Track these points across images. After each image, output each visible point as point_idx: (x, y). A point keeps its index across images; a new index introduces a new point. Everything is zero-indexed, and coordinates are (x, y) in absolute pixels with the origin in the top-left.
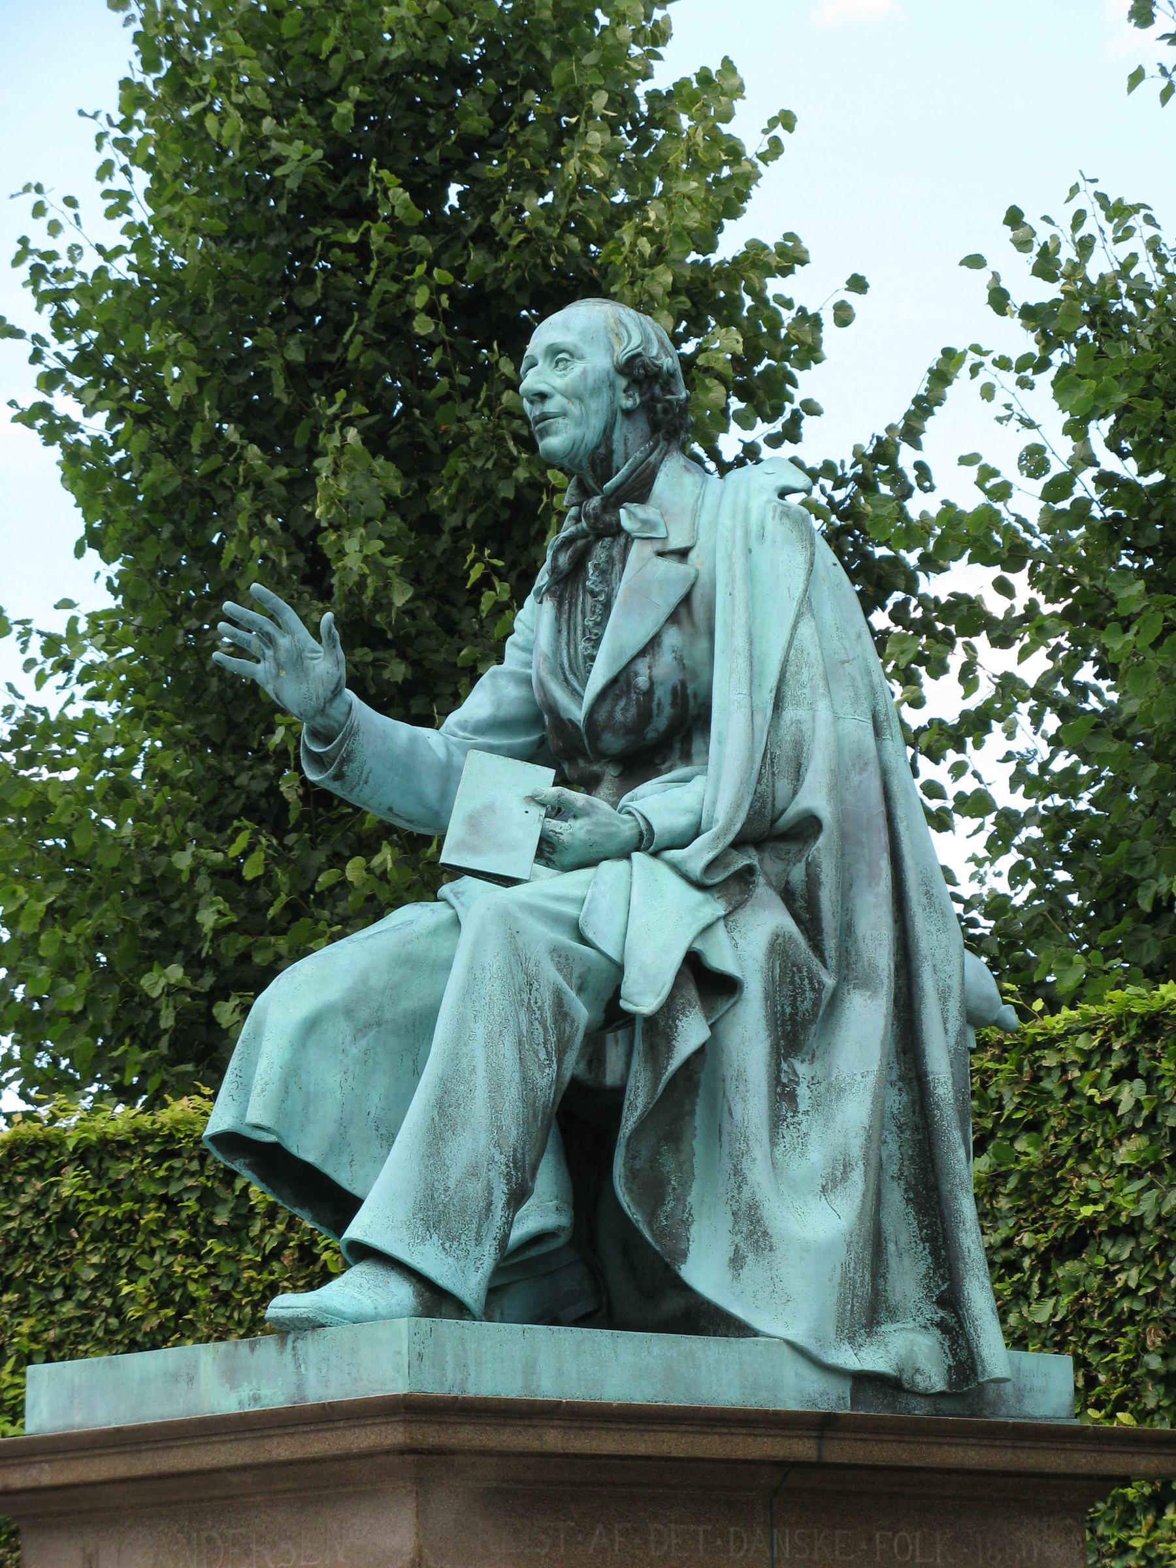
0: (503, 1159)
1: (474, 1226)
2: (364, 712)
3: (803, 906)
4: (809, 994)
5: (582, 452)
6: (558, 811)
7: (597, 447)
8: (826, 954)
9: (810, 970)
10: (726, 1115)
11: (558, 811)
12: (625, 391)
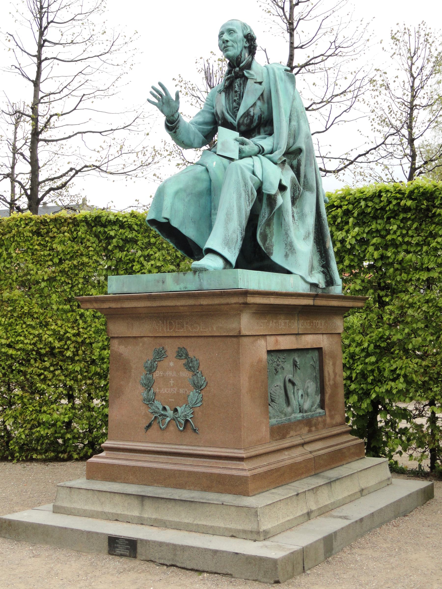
3: (297, 170)
4: (298, 192)
6: (243, 143)
11: (243, 143)
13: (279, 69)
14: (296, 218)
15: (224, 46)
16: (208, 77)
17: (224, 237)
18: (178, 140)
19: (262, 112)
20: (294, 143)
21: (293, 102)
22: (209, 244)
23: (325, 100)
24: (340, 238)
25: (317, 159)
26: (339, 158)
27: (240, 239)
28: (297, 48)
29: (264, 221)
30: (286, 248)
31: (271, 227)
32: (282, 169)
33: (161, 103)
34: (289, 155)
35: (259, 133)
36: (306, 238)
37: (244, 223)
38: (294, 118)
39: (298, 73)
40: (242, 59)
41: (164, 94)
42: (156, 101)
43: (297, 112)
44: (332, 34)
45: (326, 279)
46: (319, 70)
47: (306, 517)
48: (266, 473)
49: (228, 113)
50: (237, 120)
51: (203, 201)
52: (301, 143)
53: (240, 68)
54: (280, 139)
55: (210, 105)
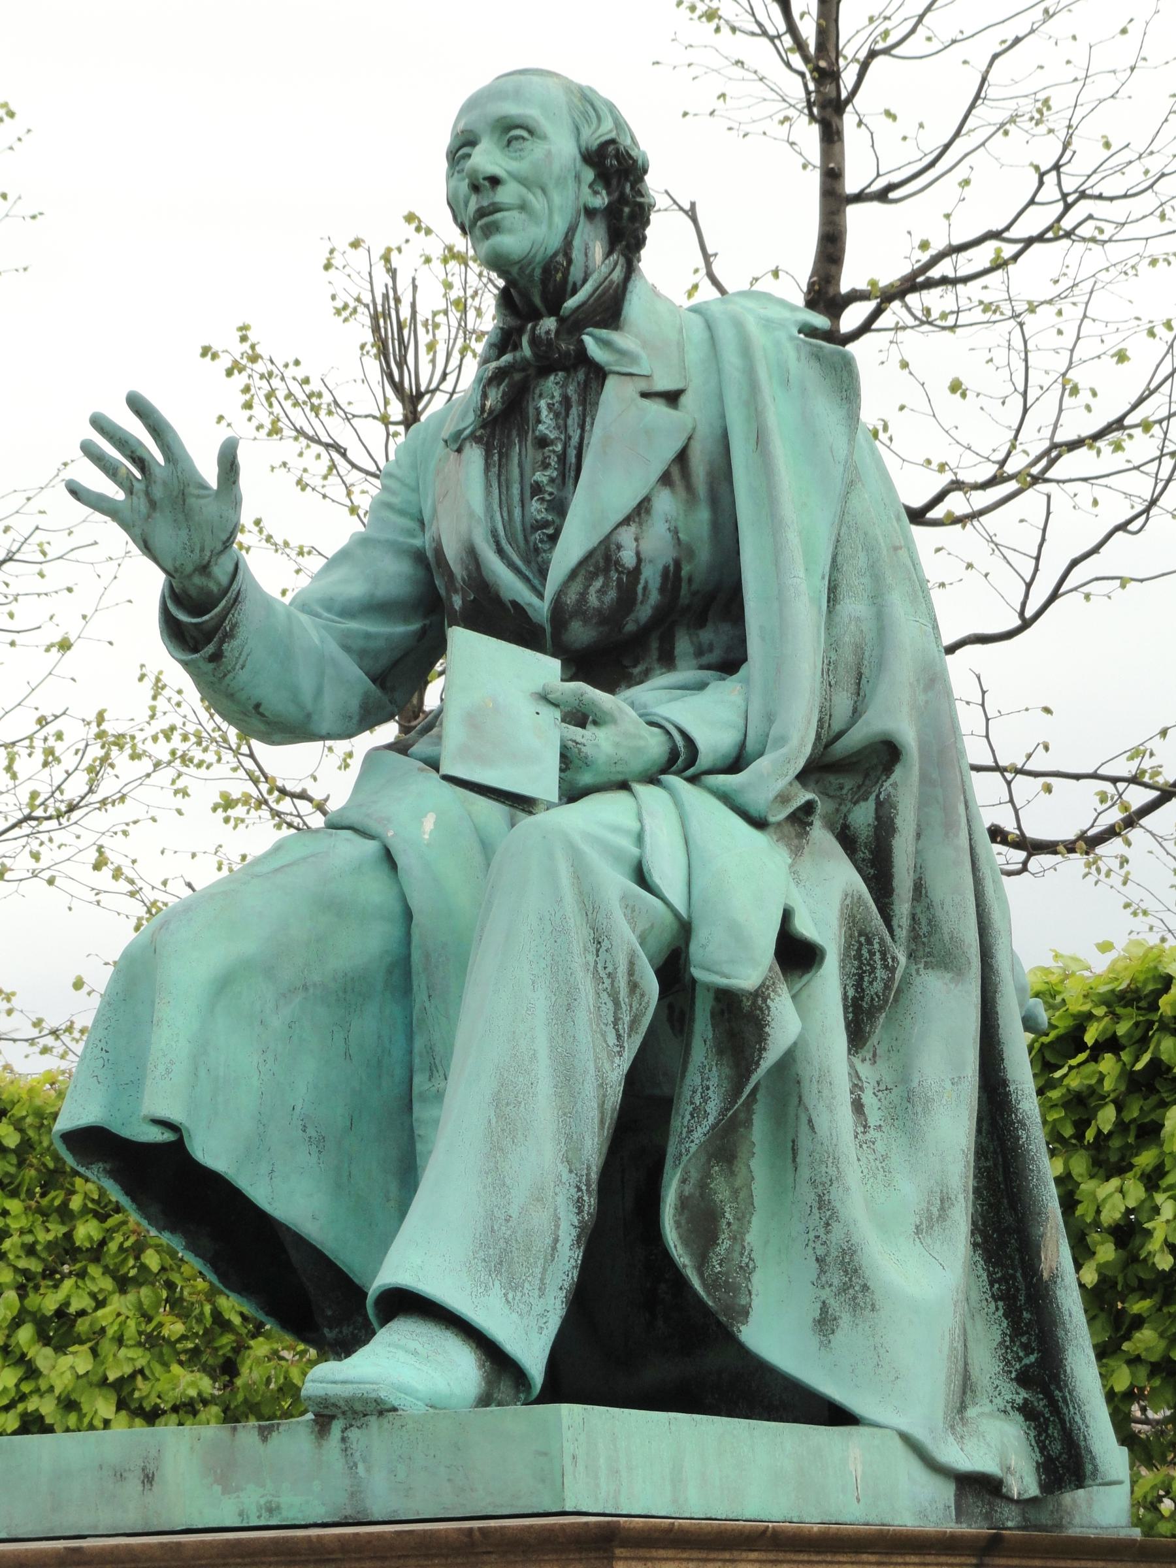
0: (573, 1179)
1: (538, 1270)
3: (874, 860)
4: (880, 973)
5: (538, 259)
6: (580, 717)
7: (555, 254)
8: (895, 923)
9: (882, 942)
10: (804, 1128)
11: (580, 717)
12: (590, 186)
13: (768, 324)
14: (874, 1118)
15: (478, 205)
16: (390, 343)
17: (484, 1226)
18: (231, 696)
19: (684, 550)
20: (856, 713)
21: (845, 497)
22: (404, 1265)
23: (1010, 468)
24: (1111, 1214)
25: (978, 780)
26: (1094, 776)
27: (568, 1234)
28: (859, 197)
29: (699, 1135)
31: (739, 1166)
32: (797, 852)
33: (142, 504)
34: (833, 779)
35: (668, 661)
36: (929, 1224)
37: (592, 1148)
38: (854, 580)
39: (866, 327)
40: (576, 273)
41: (159, 458)
42: (117, 494)
43: (870, 548)
44: (1042, 128)
45: (1043, 1449)
46: (977, 315)
49: (500, 551)
50: (550, 590)
51: (368, 1024)
52: (894, 715)
53: (561, 321)
54: (779, 696)
55: (402, 513)
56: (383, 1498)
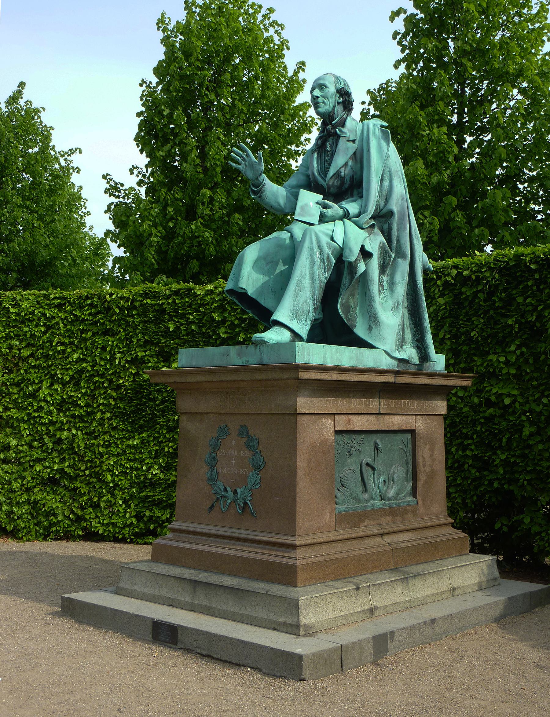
2: (267, 181)
3: (387, 235)
6: (325, 207)
11: (325, 207)
30: (369, 321)
34: (381, 219)
35: (352, 196)
36: (395, 308)
38: (387, 178)
43: (390, 171)
47: (368, 614)
48: (321, 563)
56: (266, 360)
